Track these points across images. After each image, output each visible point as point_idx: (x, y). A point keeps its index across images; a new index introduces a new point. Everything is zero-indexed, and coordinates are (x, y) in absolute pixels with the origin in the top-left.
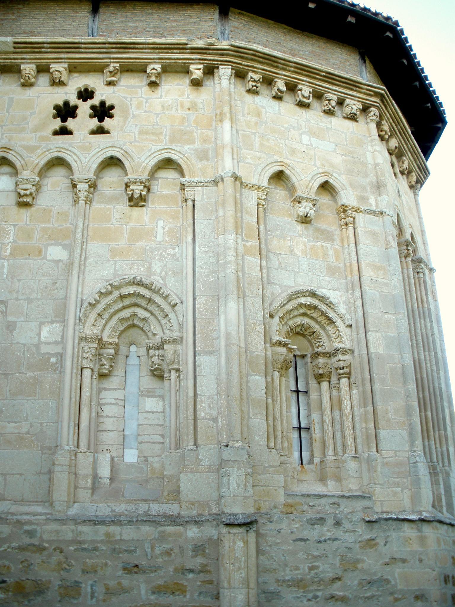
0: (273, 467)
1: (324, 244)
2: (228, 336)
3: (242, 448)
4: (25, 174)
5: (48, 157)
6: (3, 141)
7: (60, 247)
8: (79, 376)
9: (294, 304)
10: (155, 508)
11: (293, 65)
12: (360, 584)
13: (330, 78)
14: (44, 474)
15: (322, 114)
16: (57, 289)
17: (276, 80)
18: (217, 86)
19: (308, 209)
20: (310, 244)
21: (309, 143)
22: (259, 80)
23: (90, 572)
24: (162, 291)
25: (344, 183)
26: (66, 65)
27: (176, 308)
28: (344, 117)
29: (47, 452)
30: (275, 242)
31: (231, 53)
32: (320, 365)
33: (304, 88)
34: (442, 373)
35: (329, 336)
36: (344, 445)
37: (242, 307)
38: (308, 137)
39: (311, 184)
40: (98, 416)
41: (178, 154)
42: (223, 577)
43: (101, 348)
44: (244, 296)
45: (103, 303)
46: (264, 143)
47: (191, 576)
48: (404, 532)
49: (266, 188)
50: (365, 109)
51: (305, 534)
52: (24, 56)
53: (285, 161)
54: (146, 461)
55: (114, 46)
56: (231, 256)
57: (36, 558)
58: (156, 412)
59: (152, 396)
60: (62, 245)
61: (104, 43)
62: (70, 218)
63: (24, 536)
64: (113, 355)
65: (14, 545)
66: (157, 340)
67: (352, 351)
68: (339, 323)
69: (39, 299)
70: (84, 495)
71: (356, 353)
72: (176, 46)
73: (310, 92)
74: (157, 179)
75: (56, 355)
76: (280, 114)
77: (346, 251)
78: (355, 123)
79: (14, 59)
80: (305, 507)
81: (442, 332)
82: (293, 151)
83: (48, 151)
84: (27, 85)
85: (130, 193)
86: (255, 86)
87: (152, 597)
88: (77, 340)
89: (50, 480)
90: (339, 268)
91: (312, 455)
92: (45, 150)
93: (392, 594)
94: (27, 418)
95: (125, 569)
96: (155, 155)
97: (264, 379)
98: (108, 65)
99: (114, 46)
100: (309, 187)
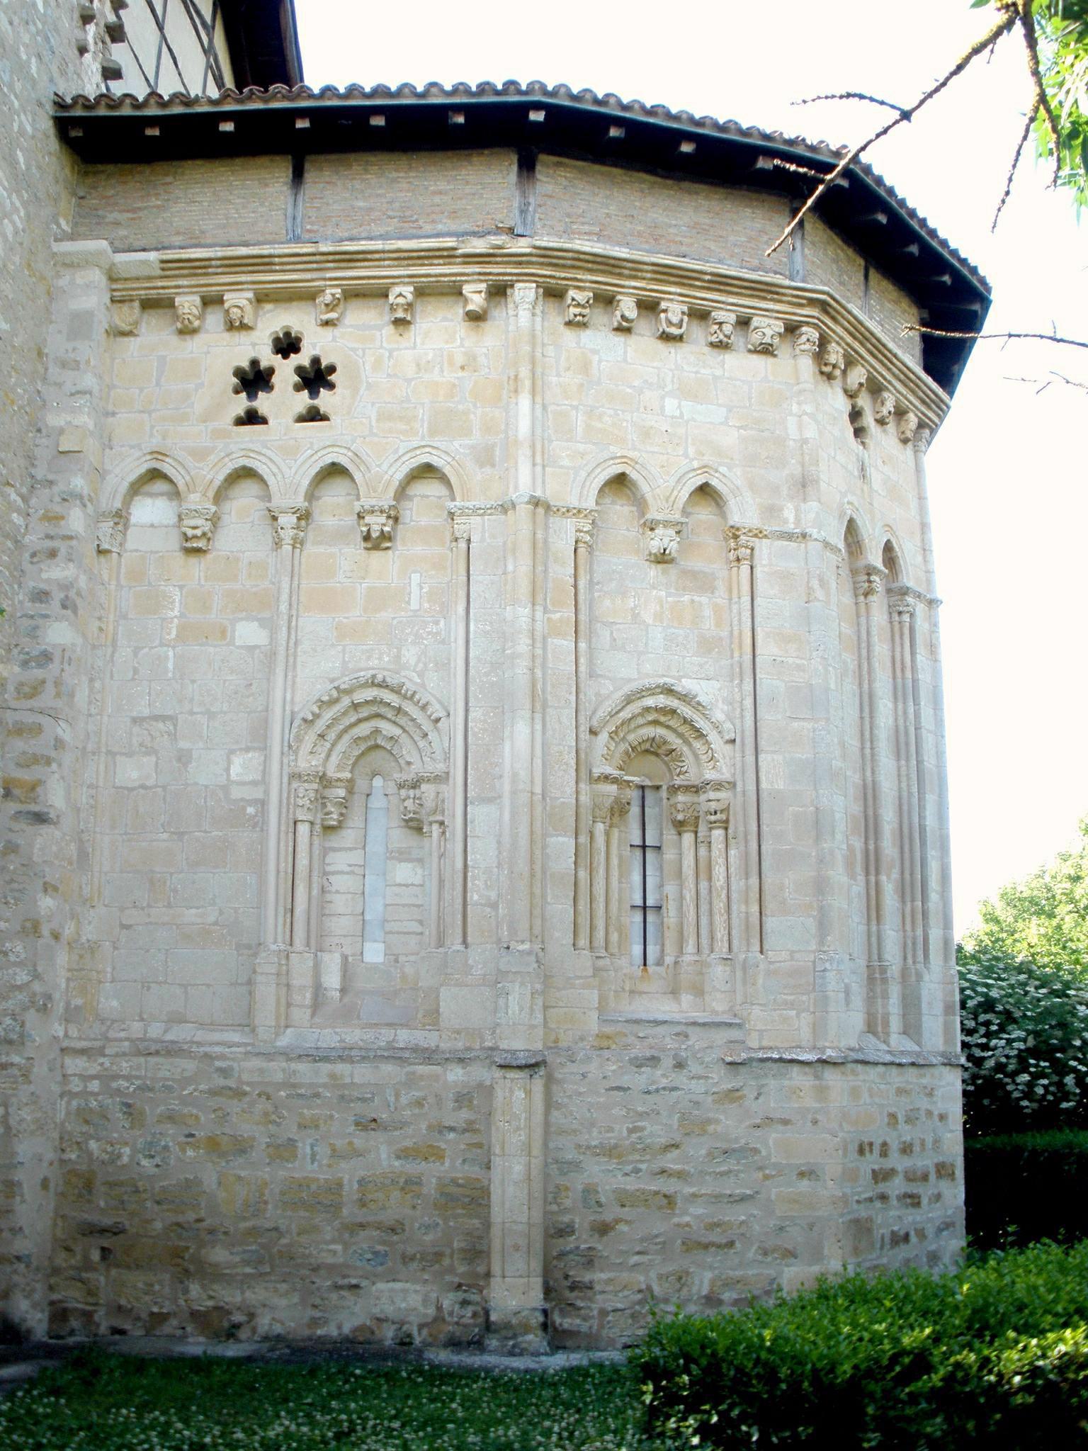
0: (580, 977)
1: (696, 598)
2: (515, 776)
3: (529, 953)
4: (194, 500)
5: (229, 467)
7: (256, 623)
8: (291, 835)
9: (635, 708)
10: (404, 1037)
11: (650, 268)
12: (709, 1154)
13: (721, 283)
14: (242, 984)
15: (707, 350)
16: (253, 694)
17: (619, 297)
18: (512, 320)
19: (666, 540)
21: (677, 413)
23: (310, 1128)
24: (417, 696)
25: (739, 483)
26: (250, 295)
27: (439, 724)
28: (750, 351)
29: (246, 952)
30: (607, 602)
31: (534, 259)
32: (680, 807)
34: (930, 799)
35: (696, 756)
36: (712, 938)
37: (538, 727)
38: (676, 402)
39: (675, 493)
40: (323, 891)
41: (443, 456)
42: (493, 1140)
43: (325, 787)
44: (545, 706)
47: (452, 1135)
48: (791, 1079)
50: (792, 329)
51: (625, 1081)
52: (180, 282)
53: (631, 454)
54: (397, 961)
55: (331, 258)
56: (523, 645)
57: (234, 1106)
58: (413, 885)
59: (410, 860)
60: (258, 620)
61: (314, 254)
63: (215, 1076)
65: (202, 1087)
66: (409, 775)
67: (733, 785)
68: (713, 737)
69: (225, 713)
70: (301, 1015)
71: (739, 788)
72: (437, 253)
73: (683, 313)
74: (410, 498)
76: (625, 360)
77: (735, 607)
78: (770, 360)
79: (163, 288)
80: (631, 1039)
81: (942, 720)
82: (646, 433)
83: (228, 455)
84: (187, 331)
85: (365, 529)
87: (397, 1163)
88: (285, 780)
89: (250, 993)
90: (721, 639)
91: (663, 951)
92: (223, 454)
93: (761, 1168)
95: (357, 1124)
96: (404, 459)
97: (571, 842)
99: (331, 258)
100: (672, 499)
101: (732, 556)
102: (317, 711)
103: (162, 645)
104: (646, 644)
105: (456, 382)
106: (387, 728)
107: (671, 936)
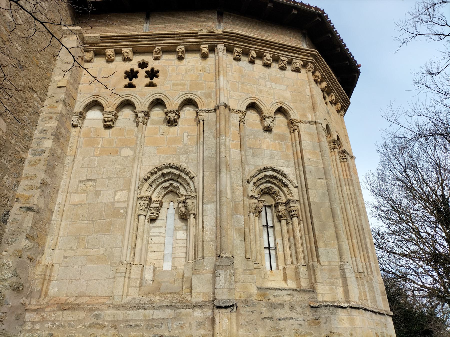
6: (95, 92)
7: (129, 149)
9: (262, 175)
13: (283, 47)
16: (126, 172)
19: (269, 122)
20: (271, 142)
21: (271, 86)
22: (240, 52)
24: (185, 170)
25: (292, 107)
28: (292, 71)
33: (267, 55)
39: (271, 109)
41: (195, 96)
45: (152, 179)
46: (244, 87)
49: (245, 112)
50: (305, 65)
53: (256, 97)
54: (176, 269)
60: (130, 148)
62: (135, 133)
64: (158, 208)
68: (290, 185)
69: (115, 178)
73: (271, 57)
75: (124, 208)
78: (299, 74)
82: (261, 91)
84: (110, 61)
85: (168, 118)
86: (238, 55)
88: (136, 199)
94: (103, 246)
96: (182, 97)
97: (243, 217)
98: (155, 48)
101: (292, 129)
102: (149, 176)
103: (94, 156)
104: (265, 155)
105: (199, 75)
106: (175, 184)
107: (281, 258)
